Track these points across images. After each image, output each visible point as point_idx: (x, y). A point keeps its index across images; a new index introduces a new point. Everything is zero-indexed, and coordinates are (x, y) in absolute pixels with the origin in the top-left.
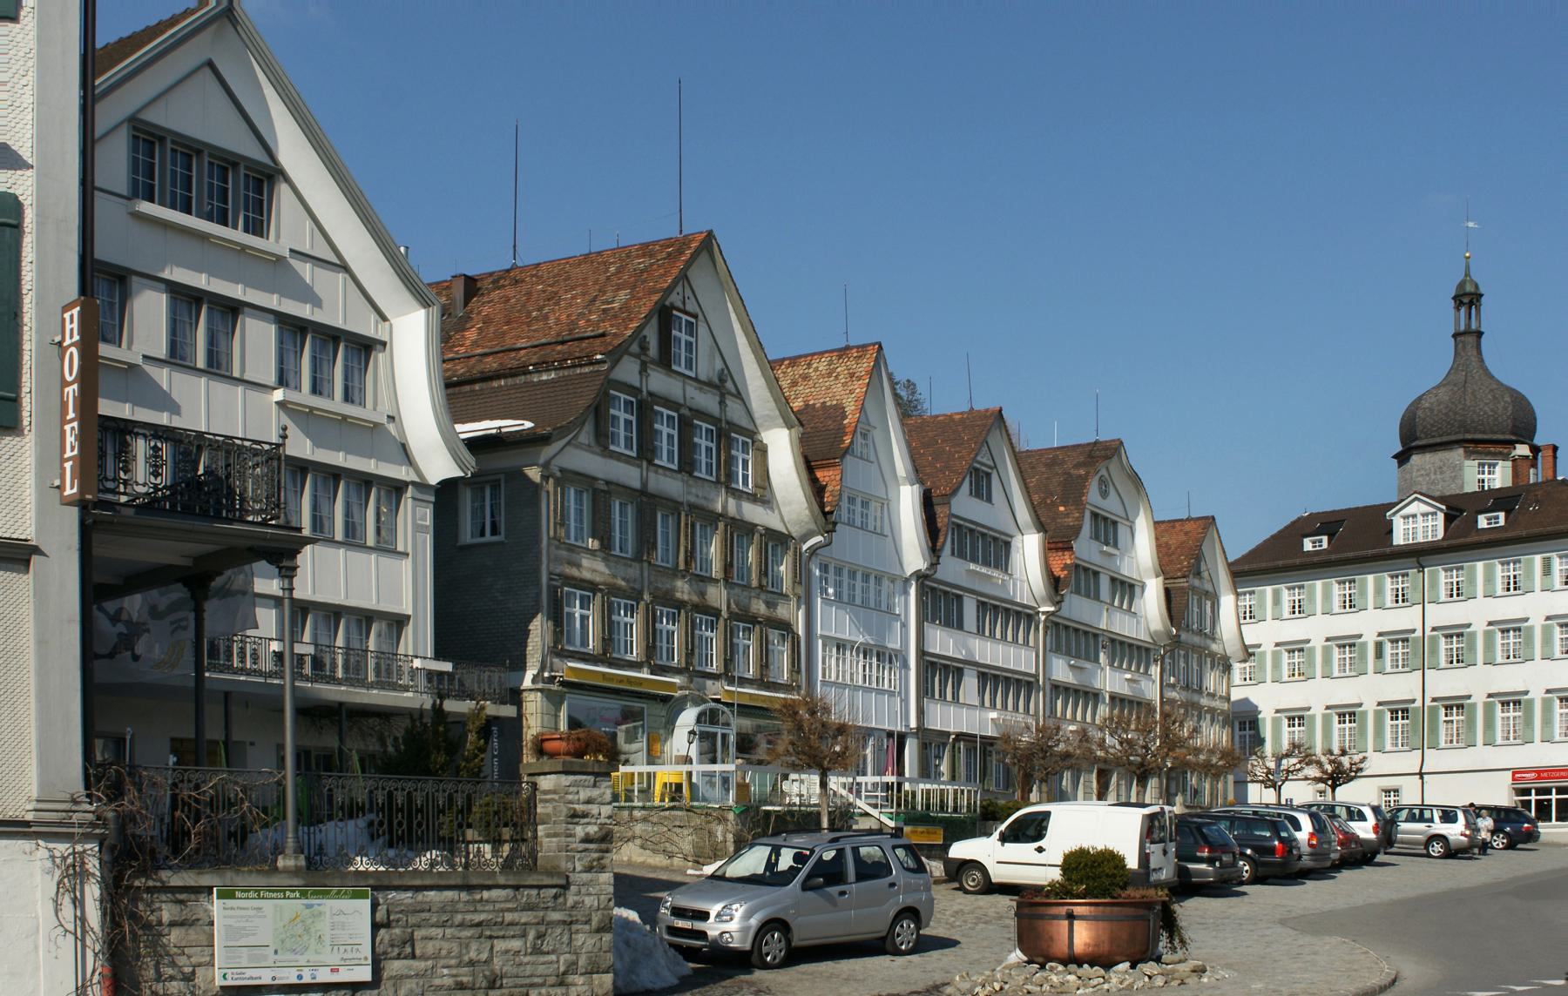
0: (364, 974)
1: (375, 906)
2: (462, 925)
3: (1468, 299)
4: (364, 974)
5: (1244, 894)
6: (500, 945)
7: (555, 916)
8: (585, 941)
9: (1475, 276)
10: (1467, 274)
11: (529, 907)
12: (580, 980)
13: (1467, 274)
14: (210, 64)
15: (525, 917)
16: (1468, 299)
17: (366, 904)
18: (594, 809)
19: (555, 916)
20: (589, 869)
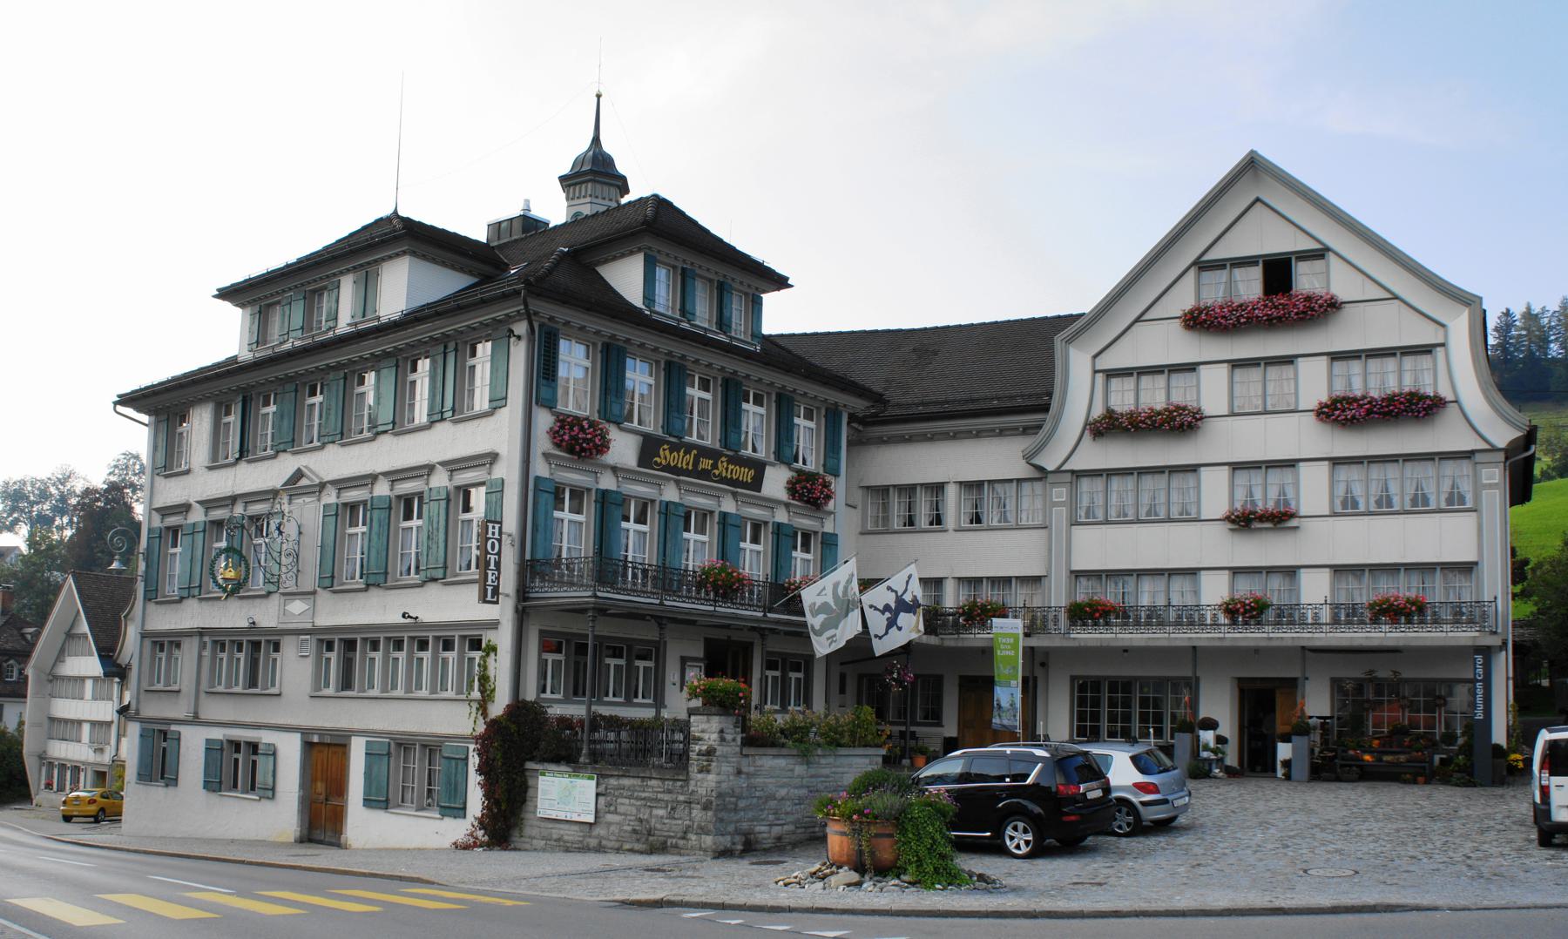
0: (591, 819)
1: (598, 785)
2: (637, 799)
3: (599, 96)
4: (591, 819)
5: (1296, 528)
6: (655, 812)
7: (681, 798)
8: (697, 813)
9: (607, 146)
10: (596, 140)
11: (670, 792)
12: (694, 837)
13: (596, 140)
14: (1258, 200)
15: (667, 797)
16: (599, 96)
17: (593, 783)
18: (706, 736)
19: (681, 798)
20: (700, 771)
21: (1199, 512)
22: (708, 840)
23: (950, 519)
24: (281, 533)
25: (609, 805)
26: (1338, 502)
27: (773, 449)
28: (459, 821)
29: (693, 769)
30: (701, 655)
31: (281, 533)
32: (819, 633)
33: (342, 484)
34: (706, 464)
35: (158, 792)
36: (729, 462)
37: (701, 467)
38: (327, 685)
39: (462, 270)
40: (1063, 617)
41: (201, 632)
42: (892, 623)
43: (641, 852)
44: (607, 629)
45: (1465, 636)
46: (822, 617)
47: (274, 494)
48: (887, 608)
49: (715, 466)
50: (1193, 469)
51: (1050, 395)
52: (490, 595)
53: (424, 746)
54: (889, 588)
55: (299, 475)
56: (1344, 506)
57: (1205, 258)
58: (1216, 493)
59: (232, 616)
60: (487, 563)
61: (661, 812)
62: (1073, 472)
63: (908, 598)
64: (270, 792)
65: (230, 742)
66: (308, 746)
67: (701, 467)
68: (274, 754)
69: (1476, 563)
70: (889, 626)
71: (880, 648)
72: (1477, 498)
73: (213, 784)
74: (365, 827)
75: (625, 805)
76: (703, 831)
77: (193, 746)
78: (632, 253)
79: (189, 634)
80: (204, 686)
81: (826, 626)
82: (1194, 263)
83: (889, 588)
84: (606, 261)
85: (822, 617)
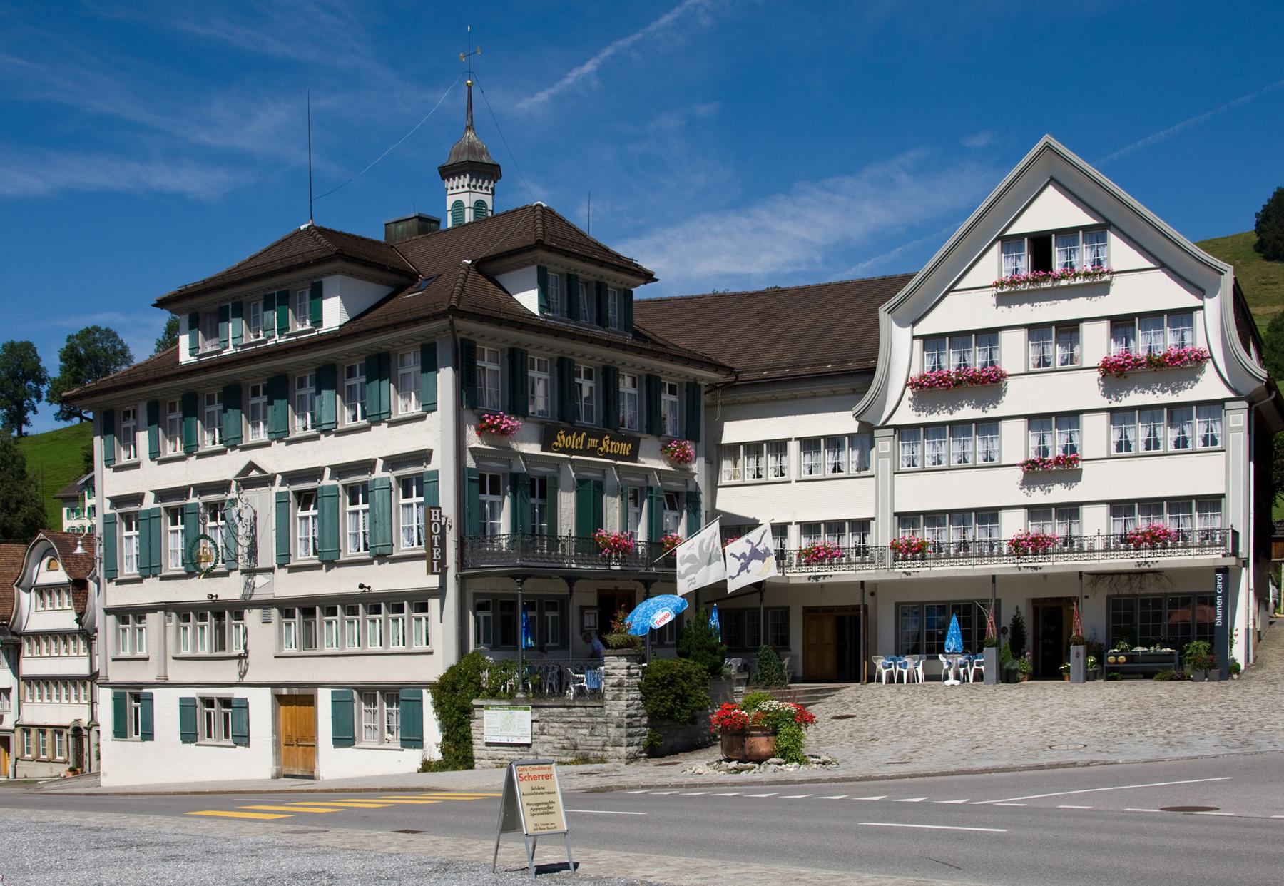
8: (612, 731)
12: (609, 748)
15: (588, 720)
20: (614, 699)
21: (1000, 459)
22: (623, 751)
23: (792, 473)
24: (241, 519)
25: (542, 729)
26: (1113, 447)
27: (645, 423)
28: (417, 751)
29: (608, 696)
30: (595, 604)
31: (241, 519)
32: (683, 577)
33: (290, 478)
34: (593, 443)
35: (133, 746)
36: (611, 440)
37: (590, 445)
38: (203, 647)
39: (381, 282)
40: (889, 554)
41: (166, 608)
42: (744, 567)
43: (572, 763)
44: (531, 586)
45: (1212, 557)
46: (688, 565)
47: (223, 486)
48: (743, 555)
49: (600, 444)
50: (997, 420)
51: (876, 359)
52: (438, 567)
53: (383, 691)
54: (748, 541)
55: (251, 466)
56: (1119, 449)
57: (1008, 233)
58: (1015, 443)
59: (196, 590)
60: (433, 542)
61: (585, 732)
62: (895, 427)
63: (760, 548)
64: (242, 739)
65: (202, 699)
66: (280, 700)
67: (590, 445)
68: (247, 707)
69: (1223, 496)
70: (741, 570)
71: (732, 587)
72: (1226, 441)
73: (189, 736)
74: (334, 764)
75: (555, 728)
76: (616, 744)
77: (166, 706)
78: (526, 265)
79: (154, 608)
80: (171, 652)
81: (688, 572)
82: (997, 239)
83: (748, 541)
84: (504, 271)
85: (688, 565)
